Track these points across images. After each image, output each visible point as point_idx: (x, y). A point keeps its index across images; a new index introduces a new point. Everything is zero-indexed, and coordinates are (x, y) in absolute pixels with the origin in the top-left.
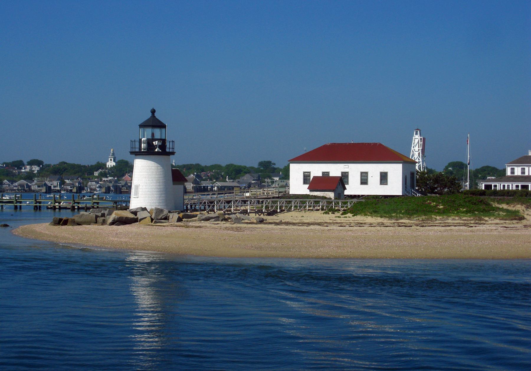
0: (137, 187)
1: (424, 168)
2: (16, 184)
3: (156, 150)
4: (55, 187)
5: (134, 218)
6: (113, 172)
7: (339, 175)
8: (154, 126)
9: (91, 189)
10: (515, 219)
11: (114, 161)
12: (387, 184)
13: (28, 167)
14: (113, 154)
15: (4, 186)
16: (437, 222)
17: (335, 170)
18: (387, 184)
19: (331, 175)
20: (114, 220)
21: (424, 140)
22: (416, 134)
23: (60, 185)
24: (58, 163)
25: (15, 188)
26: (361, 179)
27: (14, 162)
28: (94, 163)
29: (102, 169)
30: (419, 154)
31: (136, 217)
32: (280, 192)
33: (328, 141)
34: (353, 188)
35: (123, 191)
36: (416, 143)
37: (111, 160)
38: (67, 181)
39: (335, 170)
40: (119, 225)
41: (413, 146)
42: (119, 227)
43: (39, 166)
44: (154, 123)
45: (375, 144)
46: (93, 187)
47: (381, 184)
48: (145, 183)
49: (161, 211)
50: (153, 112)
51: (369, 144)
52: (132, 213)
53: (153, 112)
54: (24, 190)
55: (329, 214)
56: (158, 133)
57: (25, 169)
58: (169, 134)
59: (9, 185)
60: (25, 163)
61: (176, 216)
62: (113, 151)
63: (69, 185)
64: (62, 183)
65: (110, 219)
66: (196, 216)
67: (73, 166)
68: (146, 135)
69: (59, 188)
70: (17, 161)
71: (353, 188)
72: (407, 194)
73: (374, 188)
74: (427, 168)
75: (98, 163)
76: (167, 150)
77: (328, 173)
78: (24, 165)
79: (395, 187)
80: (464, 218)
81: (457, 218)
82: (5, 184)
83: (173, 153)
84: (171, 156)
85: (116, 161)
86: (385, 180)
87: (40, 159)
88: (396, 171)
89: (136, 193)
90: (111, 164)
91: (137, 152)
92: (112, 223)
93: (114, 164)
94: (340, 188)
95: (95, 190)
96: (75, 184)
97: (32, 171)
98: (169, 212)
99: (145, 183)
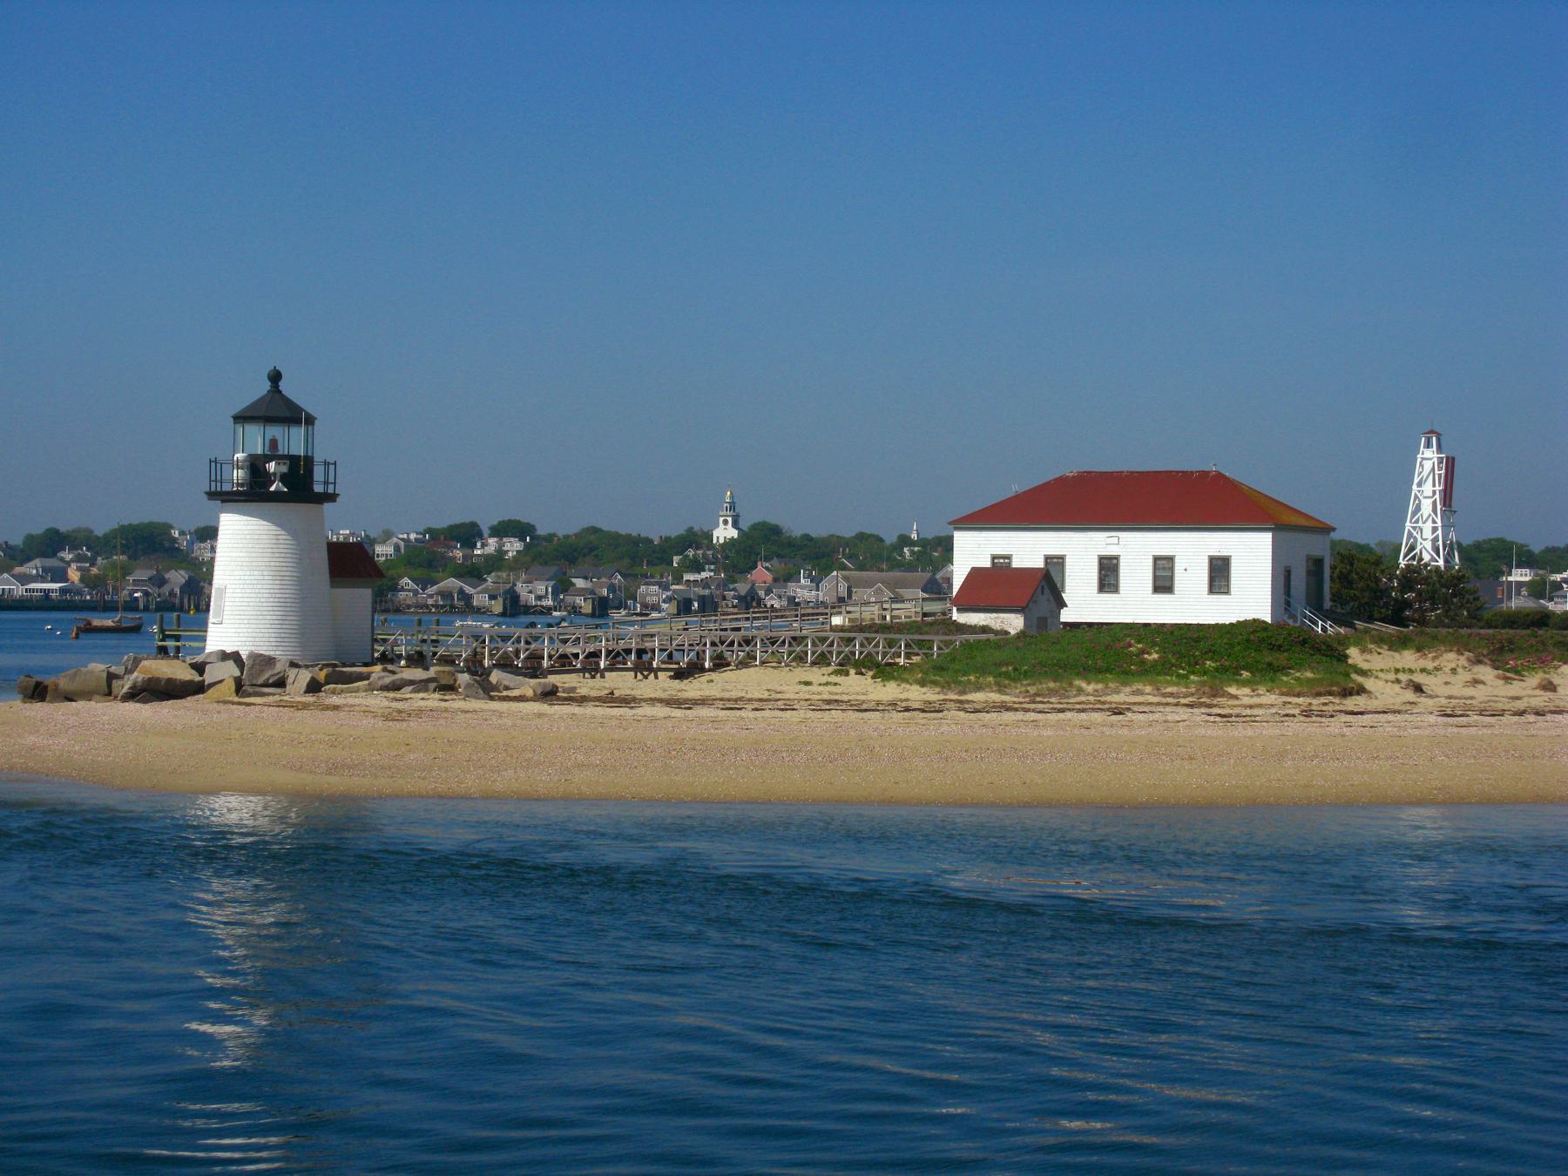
0: (222, 591)
1: (1450, 548)
2: (431, 590)
3: (284, 486)
4: (539, 598)
5: (191, 682)
6: (727, 557)
7: (1039, 563)
8: (268, 420)
9: (645, 606)
10: (1330, 694)
11: (735, 525)
12: (1228, 593)
13: (492, 541)
14: (732, 506)
15: (402, 595)
16: (1083, 698)
17: (1027, 548)
18: (1228, 593)
19: (1016, 563)
20: (133, 687)
21: (1450, 465)
22: (1428, 445)
23: (555, 593)
24: (577, 530)
25: (430, 602)
26: (1155, 578)
27: (452, 528)
28: (676, 530)
29: (697, 548)
30: (1434, 503)
31: (198, 678)
32: (925, 615)
33: (1071, 467)
34: (1083, 604)
35: (195, 598)
36: (1425, 473)
37: (726, 522)
38: (580, 583)
39: (1027, 548)
40: (145, 701)
41: (1416, 480)
42: (147, 706)
43: (523, 539)
44: (276, 409)
45: (1204, 474)
46: (650, 600)
47: (1211, 591)
48: (247, 581)
49: (270, 661)
50: (275, 377)
51: (1186, 475)
52: (195, 666)
53: (275, 377)
54: (452, 607)
55: (847, 674)
56: (294, 441)
57: (483, 545)
58: (324, 444)
59: (416, 593)
60: (486, 532)
61: (305, 676)
62: (732, 496)
63: (581, 592)
64: (563, 586)
65: (125, 686)
66: (366, 677)
67: (615, 539)
68: (255, 439)
69: (550, 603)
70: (462, 525)
71: (1083, 604)
72: (1290, 622)
73: (1192, 605)
74: (1459, 544)
75: (690, 530)
76: (318, 488)
77: (1009, 557)
78: (480, 535)
79: (1252, 598)
80: (1169, 690)
81: (1148, 689)
82: (403, 589)
83: (331, 498)
84: (327, 506)
85: (745, 525)
86: (1230, 578)
87: (524, 518)
88: (1252, 554)
89: (220, 612)
90: (724, 533)
91: (228, 493)
92: (134, 695)
93: (734, 533)
94: (1045, 599)
95: (656, 608)
96: (597, 590)
97: (501, 553)
98: (293, 665)
99: (247, 581)
